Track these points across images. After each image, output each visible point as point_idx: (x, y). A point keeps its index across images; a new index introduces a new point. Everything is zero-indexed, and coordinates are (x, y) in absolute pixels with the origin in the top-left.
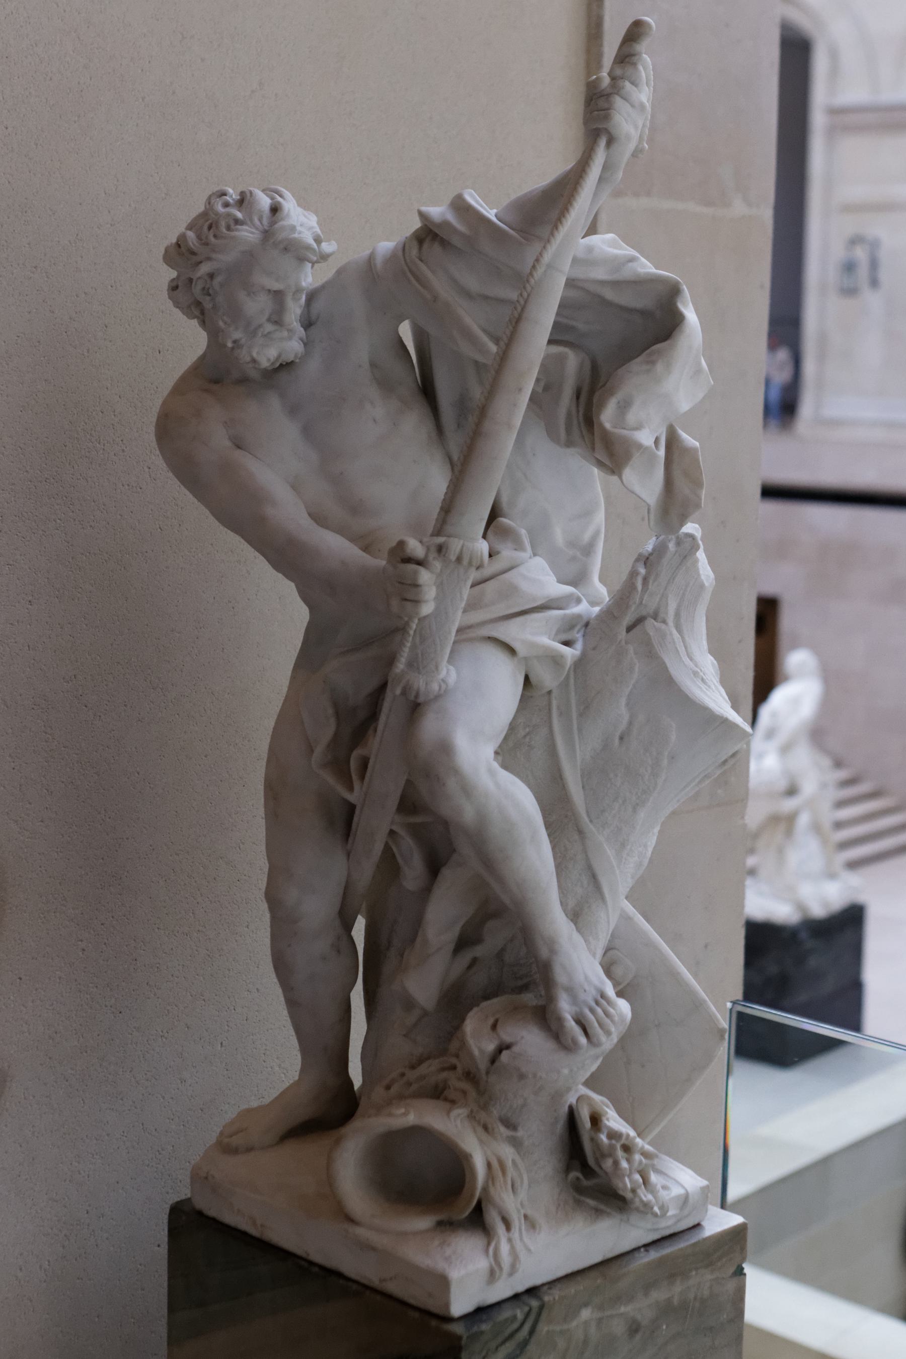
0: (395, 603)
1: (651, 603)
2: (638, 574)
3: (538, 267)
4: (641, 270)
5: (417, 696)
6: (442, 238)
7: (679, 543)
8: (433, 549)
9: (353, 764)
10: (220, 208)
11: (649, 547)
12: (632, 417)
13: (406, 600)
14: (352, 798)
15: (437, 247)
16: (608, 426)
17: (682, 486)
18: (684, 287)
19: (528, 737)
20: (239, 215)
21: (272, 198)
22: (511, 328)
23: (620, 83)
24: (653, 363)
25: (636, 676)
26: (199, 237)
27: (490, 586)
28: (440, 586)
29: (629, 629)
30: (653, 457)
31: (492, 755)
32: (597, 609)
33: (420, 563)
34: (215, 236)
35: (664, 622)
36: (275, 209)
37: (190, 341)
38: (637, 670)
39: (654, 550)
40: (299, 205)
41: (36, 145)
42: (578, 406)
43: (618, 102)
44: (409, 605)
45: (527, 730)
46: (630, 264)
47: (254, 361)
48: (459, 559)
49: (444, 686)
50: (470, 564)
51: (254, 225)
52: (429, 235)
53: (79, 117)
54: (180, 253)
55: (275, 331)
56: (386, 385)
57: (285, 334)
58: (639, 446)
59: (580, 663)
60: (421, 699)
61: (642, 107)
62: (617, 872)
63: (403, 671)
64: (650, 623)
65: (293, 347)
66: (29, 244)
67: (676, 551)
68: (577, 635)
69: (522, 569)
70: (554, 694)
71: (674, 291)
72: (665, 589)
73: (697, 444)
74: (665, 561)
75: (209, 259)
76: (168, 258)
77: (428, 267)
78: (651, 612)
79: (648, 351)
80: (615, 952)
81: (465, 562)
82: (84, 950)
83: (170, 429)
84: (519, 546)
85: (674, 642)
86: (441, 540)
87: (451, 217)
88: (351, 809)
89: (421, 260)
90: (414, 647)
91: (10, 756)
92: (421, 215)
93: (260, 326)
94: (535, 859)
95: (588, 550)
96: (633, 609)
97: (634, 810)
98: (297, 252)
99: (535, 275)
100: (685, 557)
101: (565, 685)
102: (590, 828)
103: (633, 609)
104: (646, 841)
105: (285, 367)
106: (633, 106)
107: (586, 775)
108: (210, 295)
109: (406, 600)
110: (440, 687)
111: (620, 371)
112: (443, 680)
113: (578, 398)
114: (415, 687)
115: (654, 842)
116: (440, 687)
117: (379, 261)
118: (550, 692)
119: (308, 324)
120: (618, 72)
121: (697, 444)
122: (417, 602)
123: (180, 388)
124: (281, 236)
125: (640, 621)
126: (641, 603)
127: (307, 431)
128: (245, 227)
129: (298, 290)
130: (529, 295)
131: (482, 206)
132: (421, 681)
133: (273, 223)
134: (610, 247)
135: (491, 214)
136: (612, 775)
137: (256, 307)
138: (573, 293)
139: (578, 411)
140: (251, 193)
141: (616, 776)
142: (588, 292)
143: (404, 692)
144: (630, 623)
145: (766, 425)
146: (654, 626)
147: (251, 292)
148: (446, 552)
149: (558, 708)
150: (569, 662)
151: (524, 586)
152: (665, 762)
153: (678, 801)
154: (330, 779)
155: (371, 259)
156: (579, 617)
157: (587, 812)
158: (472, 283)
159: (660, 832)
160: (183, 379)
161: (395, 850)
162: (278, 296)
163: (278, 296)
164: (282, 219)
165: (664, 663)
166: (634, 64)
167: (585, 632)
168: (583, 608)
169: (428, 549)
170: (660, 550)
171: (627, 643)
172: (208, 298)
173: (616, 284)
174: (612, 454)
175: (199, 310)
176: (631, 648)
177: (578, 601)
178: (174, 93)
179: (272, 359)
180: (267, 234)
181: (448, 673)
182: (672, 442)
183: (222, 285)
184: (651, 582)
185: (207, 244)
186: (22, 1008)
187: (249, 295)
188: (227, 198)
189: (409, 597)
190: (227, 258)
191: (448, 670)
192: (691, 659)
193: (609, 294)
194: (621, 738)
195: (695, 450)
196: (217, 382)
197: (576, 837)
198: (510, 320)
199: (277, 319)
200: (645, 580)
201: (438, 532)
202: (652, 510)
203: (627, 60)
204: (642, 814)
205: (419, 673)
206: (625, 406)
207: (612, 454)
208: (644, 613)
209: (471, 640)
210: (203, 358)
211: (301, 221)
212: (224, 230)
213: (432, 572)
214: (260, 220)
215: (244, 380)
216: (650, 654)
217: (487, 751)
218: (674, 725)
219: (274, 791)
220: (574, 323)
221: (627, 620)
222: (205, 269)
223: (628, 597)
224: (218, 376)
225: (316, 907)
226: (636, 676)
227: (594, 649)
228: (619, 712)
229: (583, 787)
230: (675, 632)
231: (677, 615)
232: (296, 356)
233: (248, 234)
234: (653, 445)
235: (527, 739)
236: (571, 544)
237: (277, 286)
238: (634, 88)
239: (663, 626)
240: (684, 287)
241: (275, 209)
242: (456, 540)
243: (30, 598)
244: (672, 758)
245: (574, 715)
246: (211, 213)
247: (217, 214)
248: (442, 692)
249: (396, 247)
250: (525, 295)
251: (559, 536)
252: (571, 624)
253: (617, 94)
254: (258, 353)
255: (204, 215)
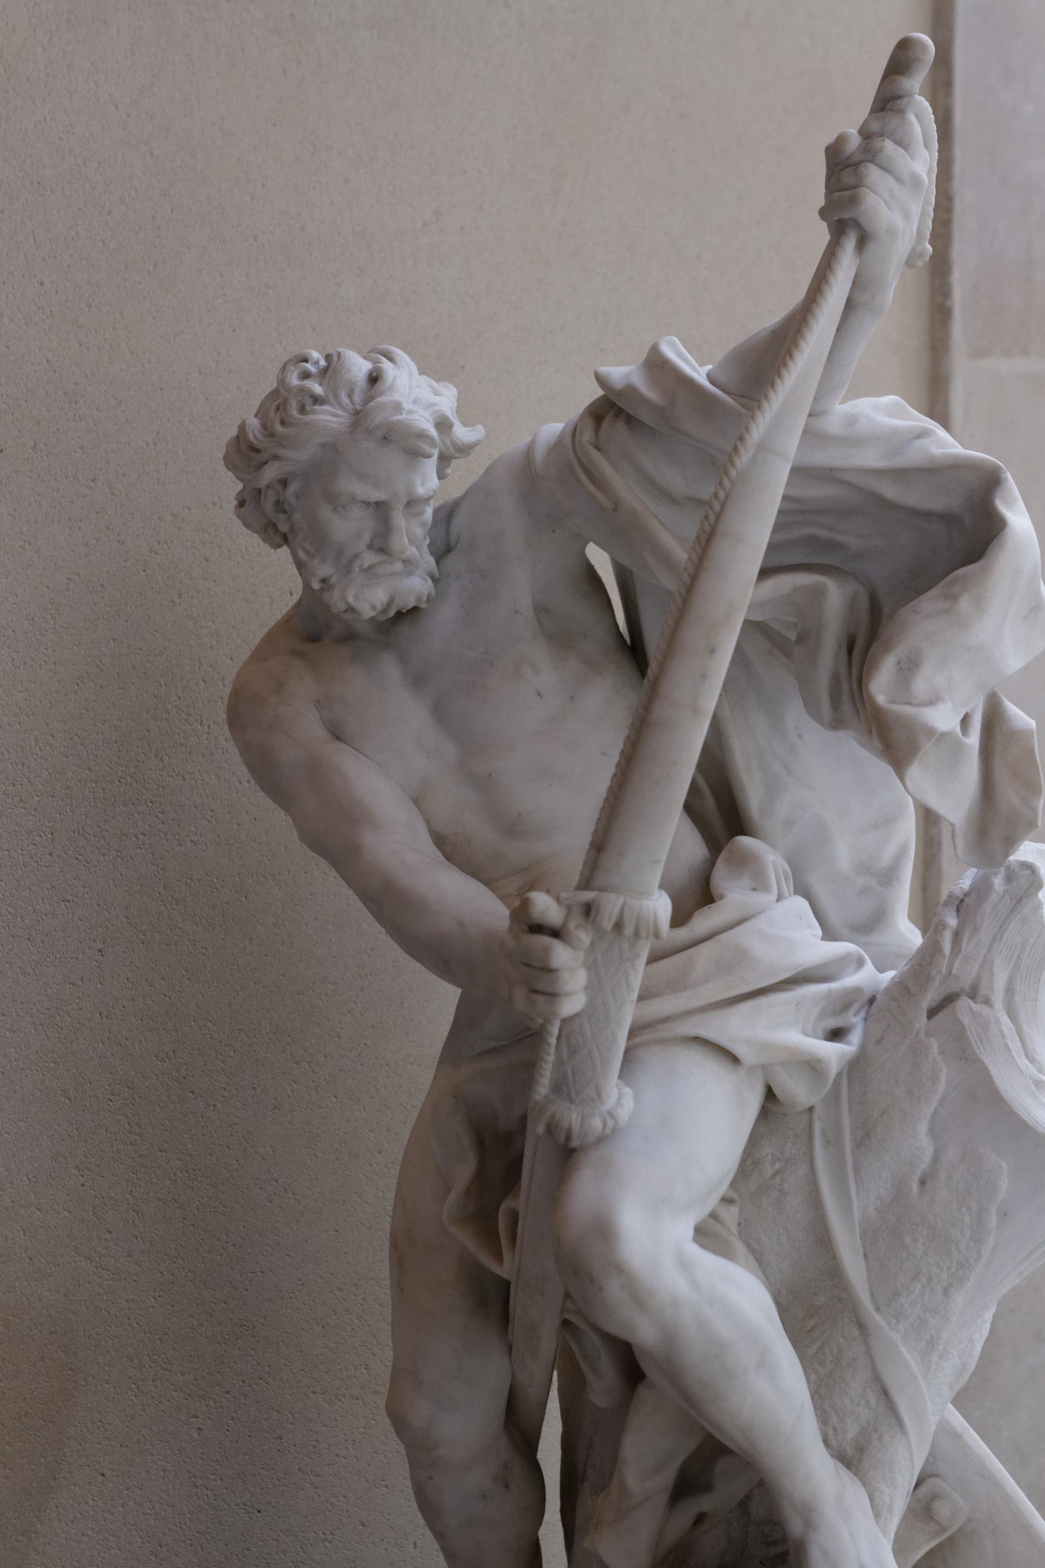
0: (519, 996)
1: (966, 972)
2: (944, 926)
3: (742, 450)
4: (937, 451)
5: (568, 1138)
6: (628, 414)
7: (1009, 879)
8: (577, 911)
9: (502, 1223)
10: (294, 381)
11: (966, 884)
12: (920, 685)
13: (536, 991)
14: (504, 1271)
15: (621, 426)
16: (881, 699)
17: (1008, 794)
18: (1009, 475)
19: (778, 1177)
20: (318, 389)
21: (376, 362)
22: (698, 549)
23: (876, 143)
24: (954, 597)
25: (942, 1087)
26: (264, 426)
27: (704, 953)
28: (592, 967)
29: (932, 1013)
30: (957, 749)
31: (690, 1232)
32: (890, 975)
33: (556, 933)
34: (283, 423)
35: (987, 1002)
36: (374, 379)
37: (270, 582)
38: (943, 1077)
39: (972, 887)
40: (422, 372)
41: (90, 307)
42: (850, 665)
43: (873, 173)
44: (540, 999)
45: (778, 1166)
46: (919, 443)
47: (351, 609)
48: (618, 926)
49: (610, 1123)
50: (637, 934)
51: (340, 405)
52: (610, 410)
53: (155, 265)
54: (245, 454)
55: (380, 563)
56: (560, 638)
57: (399, 566)
58: (930, 732)
59: (855, 1066)
60: (575, 1143)
61: (916, 182)
62: (923, 1386)
63: (546, 1097)
64: (964, 1004)
65: (416, 586)
66: (82, 448)
67: (1006, 891)
68: (855, 1020)
69: (758, 923)
70: (818, 1112)
71: (990, 482)
72: (989, 951)
73: (1033, 723)
74: (987, 907)
75: (276, 457)
76: (229, 463)
77: (608, 458)
78: (967, 987)
79: (947, 579)
80: (938, 1480)
81: (628, 931)
82: (199, 1429)
83: (243, 711)
84: (760, 883)
85: (1003, 1036)
86: (588, 896)
87: (639, 382)
88: (504, 1288)
89: (598, 448)
90: (559, 1062)
91: (77, 1168)
92: (601, 380)
93: (357, 556)
94: (773, 1393)
95: (888, 877)
96: (937, 982)
97: (946, 1292)
98: (406, 444)
99: (738, 463)
100: (1020, 899)
101: (834, 1096)
102: (877, 1320)
103: (937, 982)
104: (969, 1330)
105: (403, 617)
106: (898, 179)
107: (870, 1237)
108: (285, 512)
109: (536, 991)
110: (605, 1124)
111: (905, 611)
112: (610, 1113)
113: (850, 651)
114: (565, 1125)
115: (986, 1332)
116: (605, 1124)
117: (539, 453)
118: (811, 1109)
119: (443, 551)
120: (875, 126)
121: (1033, 723)
122: (553, 996)
123: (260, 655)
124: (379, 419)
125: (948, 1000)
126: (950, 973)
127: (439, 711)
128: (326, 407)
129: (413, 503)
130: (727, 496)
131: (686, 361)
132: (574, 1116)
133: (368, 398)
134: (892, 416)
135: (699, 373)
136: (908, 1240)
137: (348, 527)
138: (815, 491)
139: (850, 673)
140: (339, 354)
141: (915, 1240)
142: (860, 489)
143: (550, 1130)
144: (934, 1004)
145: (721, 897)
146: (971, 1008)
147: (338, 503)
148: (596, 916)
149: (824, 1133)
150: (833, 1071)
151: (760, 950)
152: (993, 1220)
153: (1021, 1274)
154: (472, 1245)
155: (529, 451)
156: (857, 991)
157: (872, 1295)
158: (675, 480)
159: (995, 1316)
160: (269, 637)
161: (574, 1347)
162: (381, 510)
163: (381, 510)
164: (383, 393)
165: (986, 1068)
166: (901, 112)
167: (867, 1013)
168: (869, 977)
169: (569, 909)
170: (981, 889)
171: (928, 1035)
172: (282, 517)
173: (901, 474)
174: (894, 742)
175: (276, 534)
176: (934, 1045)
177: (860, 963)
178: (303, 228)
179: (379, 605)
180: (358, 417)
181: (619, 1099)
182: (994, 721)
183: (298, 496)
184: (965, 940)
185: (272, 435)
186: (107, 1514)
187: (335, 509)
188: (308, 365)
189: (540, 987)
190: (301, 455)
191: (621, 1095)
192: (1031, 1059)
193: (890, 491)
194: (923, 1183)
195: (1029, 733)
196: (314, 638)
197: (856, 1333)
198: (698, 538)
199: (381, 544)
200: (957, 935)
201: (586, 884)
202: (957, 832)
203: (889, 106)
204: (959, 1299)
205: (572, 1102)
206: (909, 667)
207: (894, 742)
208: (955, 988)
209: (665, 1042)
210: (298, 604)
211: (417, 395)
212: (295, 413)
213: (575, 948)
214: (350, 395)
215: (350, 637)
216: (963, 1052)
217: (683, 1229)
218: (1005, 1166)
219: (404, 1248)
220: (839, 537)
221: (929, 999)
222: (271, 473)
223: (930, 964)
224: (316, 632)
225: (466, 1426)
226: (942, 1087)
227: (879, 1042)
228: (920, 1142)
229: (865, 1256)
230: (1005, 1020)
231: (1010, 991)
232: (419, 599)
233: (330, 418)
234: (958, 729)
235: (777, 1180)
236: (862, 868)
237: (376, 495)
238: (901, 151)
239: (985, 1010)
240: (1009, 475)
241: (374, 379)
242: (613, 896)
243: (101, 946)
244: (1004, 1214)
245: (848, 1146)
246: (282, 391)
247: (288, 390)
248: (608, 1131)
249: (563, 431)
250: (722, 495)
251: (844, 854)
252: (845, 1002)
253: (872, 162)
254: (356, 596)
255: (275, 392)
